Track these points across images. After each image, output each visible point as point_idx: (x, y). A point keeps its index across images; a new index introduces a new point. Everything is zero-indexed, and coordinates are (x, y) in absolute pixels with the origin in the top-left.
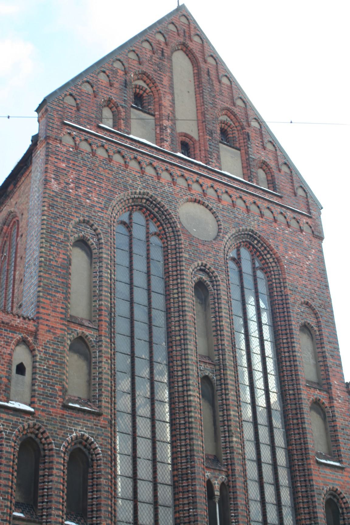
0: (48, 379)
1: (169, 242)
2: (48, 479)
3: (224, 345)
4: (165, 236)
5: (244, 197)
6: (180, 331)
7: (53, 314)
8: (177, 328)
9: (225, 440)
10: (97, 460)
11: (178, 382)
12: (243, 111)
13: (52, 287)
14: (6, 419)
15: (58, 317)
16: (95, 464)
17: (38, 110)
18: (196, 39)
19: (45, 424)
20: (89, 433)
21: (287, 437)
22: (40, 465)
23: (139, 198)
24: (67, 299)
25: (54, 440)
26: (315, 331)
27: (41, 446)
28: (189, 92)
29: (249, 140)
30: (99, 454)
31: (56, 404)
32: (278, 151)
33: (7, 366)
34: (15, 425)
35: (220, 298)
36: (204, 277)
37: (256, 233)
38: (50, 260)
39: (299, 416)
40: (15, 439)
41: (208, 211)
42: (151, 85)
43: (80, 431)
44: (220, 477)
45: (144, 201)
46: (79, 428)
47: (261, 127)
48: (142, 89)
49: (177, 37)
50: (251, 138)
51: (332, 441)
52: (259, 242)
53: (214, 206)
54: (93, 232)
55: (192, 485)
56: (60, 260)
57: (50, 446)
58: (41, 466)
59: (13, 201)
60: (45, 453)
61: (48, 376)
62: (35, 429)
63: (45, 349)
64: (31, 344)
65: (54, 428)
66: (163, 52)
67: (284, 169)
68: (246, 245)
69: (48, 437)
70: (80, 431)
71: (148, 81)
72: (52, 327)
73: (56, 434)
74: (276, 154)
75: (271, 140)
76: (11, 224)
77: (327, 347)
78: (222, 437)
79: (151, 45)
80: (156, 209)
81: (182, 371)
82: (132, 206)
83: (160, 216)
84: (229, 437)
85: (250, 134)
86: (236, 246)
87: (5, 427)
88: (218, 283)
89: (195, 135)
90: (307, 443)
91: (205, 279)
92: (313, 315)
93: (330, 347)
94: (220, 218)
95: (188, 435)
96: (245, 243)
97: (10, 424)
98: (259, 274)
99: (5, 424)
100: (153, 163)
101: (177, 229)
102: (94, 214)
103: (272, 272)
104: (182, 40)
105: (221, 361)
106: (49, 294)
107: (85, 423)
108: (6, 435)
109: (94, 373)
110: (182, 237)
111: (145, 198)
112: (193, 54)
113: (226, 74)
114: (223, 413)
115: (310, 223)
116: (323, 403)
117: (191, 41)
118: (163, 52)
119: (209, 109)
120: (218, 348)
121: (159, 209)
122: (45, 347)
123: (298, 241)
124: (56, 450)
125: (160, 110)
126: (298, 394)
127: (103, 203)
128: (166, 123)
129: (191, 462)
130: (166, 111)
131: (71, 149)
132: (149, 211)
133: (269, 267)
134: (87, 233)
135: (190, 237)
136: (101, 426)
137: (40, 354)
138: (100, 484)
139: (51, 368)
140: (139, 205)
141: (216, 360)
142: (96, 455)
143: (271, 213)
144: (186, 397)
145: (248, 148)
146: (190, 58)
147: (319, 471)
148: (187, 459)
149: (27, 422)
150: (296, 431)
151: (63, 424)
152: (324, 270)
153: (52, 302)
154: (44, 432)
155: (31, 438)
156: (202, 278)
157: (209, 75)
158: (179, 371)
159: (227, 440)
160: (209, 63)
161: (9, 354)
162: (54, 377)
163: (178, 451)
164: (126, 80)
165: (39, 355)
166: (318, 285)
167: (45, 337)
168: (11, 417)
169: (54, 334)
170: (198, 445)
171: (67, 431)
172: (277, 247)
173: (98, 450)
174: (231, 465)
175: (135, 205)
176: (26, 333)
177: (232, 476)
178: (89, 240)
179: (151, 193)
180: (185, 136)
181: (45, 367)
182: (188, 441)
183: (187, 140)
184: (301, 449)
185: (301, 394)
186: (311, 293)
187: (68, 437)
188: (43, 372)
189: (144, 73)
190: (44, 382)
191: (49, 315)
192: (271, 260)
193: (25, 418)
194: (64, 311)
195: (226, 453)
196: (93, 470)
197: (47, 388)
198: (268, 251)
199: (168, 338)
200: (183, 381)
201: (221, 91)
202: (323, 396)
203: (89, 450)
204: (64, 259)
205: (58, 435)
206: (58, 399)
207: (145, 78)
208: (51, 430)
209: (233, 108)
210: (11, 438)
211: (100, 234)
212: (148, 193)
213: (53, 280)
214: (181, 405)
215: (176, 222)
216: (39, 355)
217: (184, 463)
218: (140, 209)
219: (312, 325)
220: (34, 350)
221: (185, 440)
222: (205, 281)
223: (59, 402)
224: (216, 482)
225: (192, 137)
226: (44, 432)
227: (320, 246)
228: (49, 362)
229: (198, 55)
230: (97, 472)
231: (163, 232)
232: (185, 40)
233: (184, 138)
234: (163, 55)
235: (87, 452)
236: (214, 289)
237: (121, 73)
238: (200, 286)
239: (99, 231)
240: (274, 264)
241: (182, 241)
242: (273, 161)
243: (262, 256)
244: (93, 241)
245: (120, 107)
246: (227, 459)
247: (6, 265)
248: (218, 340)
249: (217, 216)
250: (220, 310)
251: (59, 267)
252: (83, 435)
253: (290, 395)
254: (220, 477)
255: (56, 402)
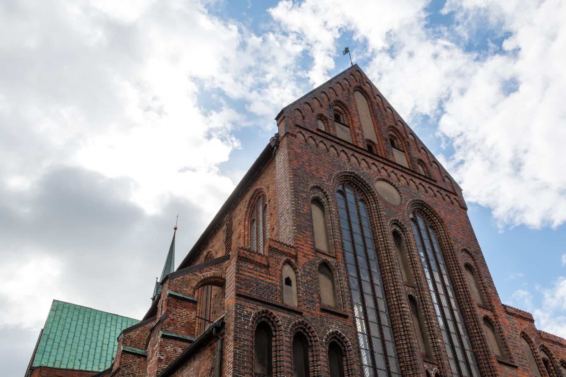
0: (308, 289)
1: (371, 205)
2: (317, 364)
3: (419, 273)
4: (367, 201)
5: (413, 180)
6: (388, 263)
7: (306, 245)
8: (386, 261)
9: (432, 341)
10: (349, 351)
11: (393, 298)
12: (402, 128)
13: (303, 227)
14: (283, 317)
15: (309, 247)
16: (348, 354)
17: (277, 119)
18: (367, 85)
19: (310, 322)
20: (341, 330)
21: (471, 342)
22: (309, 353)
23: (348, 175)
24: (313, 235)
25: (318, 334)
26: (475, 269)
27: (308, 339)
28: (367, 115)
29: (409, 146)
30: (349, 346)
31: (316, 308)
32: (428, 154)
33: (280, 278)
34: (290, 321)
35: (411, 243)
36: (397, 229)
37: (425, 202)
38: (299, 210)
39: (477, 327)
40: (290, 331)
41: (392, 187)
42: (345, 109)
43: (334, 328)
44: (434, 369)
45: (352, 178)
46: (334, 326)
47: (415, 139)
48: (339, 112)
49: (356, 83)
50: (410, 145)
51: (503, 347)
52: (427, 208)
53: (396, 184)
54: (323, 194)
55: (417, 374)
56: (306, 210)
57: (315, 338)
58: (310, 354)
59: (259, 182)
60: (312, 344)
61: (308, 288)
62: (303, 325)
63: (303, 269)
64: (294, 264)
65: (317, 325)
66: (349, 90)
67: (434, 165)
68: (419, 211)
69: (313, 332)
70: (334, 328)
71: (343, 107)
72: (307, 254)
73: (319, 329)
74: (427, 155)
75: (422, 146)
76: (257, 198)
77: (485, 280)
78: (430, 339)
79: (341, 85)
80: (360, 184)
81: (395, 290)
82: (344, 181)
83: (363, 188)
84: (435, 339)
85: (409, 142)
86: (413, 211)
87: (283, 322)
88: (407, 233)
89: (375, 141)
90: (488, 347)
91: (398, 230)
92: (471, 259)
93: (487, 280)
94: (401, 191)
95: (407, 336)
96: (418, 210)
97: (286, 320)
98: (430, 231)
99: (283, 320)
100: (355, 154)
101: (376, 196)
102: (322, 182)
103: (439, 229)
104: (358, 84)
105: (419, 284)
106: (301, 232)
107: (337, 323)
108: (284, 328)
109: (337, 288)
110: (380, 201)
111: (352, 176)
112: (366, 93)
113: (388, 106)
114: (427, 321)
115: (457, 199)
116: (491, 319)
117: (365, 86)
118: (349, 90)
119: (382, 125)
120: (415, 276)
121: (362, 183)
122: (304, 268)
123: (452, 209)
124: (320, 341)
125: (353, 124)
126: (474, 311)
127: (328, 176)
128: (357, 131)
129: (413, 356)
130: (356, 125)
131: (303, 142)
132: (355, 185)
133: (436, 226)
134: (319, 194)
135: (385, 202)
136: (348, 326)
137: (301, 271)
138: (354, 369)
139: (309, 282)
140: (348, 181)
141: (415, 284)
142: (348, 347)
143: (432, 191)
144: (401, 308)
145: (410, 150)
146: (364, 96)
147: (500, 368)
148: (410, 354)
149: (297, 319)
150: (478, 338)
151: (322, 322)
152: (472, 229)
153: (304, 237)
154: (310, 328)
155: (300, 332)
156: (396, 229)
157: (378, 106)
158: (393, 290)
159: (434, 341)
160: (377, 99)
161: (280, 270)
162: (312, 289)
163: (401, 348)
164: (330, 104)
165: (300, 272)
166: (470, 239)
167: (302, 260)
168: (286, 315)
169: (308, 258)
170: (415, 343)
171: (326, 328)
172: (440, 212)
173: (349, 343)
174: (440, 359)
175: (346, 181)
176: (289, 256)
177: (443, 368)
178: (321, 199)
179: (356, 173)
180: (369, 142)
181: (305, 281)
182: (408, 340)
183: (371, 144)
184: (484, 351)
185: (476, 311)
186: (467, 243)
187: (327, 332)
188: (304, 284)
189: (339, 101)
190: (306, 292)
191: (303, 245)
192: (437, 221)
193: (296, 316)
194: (312, 243)
195: (435, 351)
196: (346, 358)
197: (308, 295)
198: (434, 215)
199: (380, 268)
200: (396, 297)
201: (387, 116)
202: (489, 314)
203: (308, 333)
204: (308, 210)
205: (320, 330)
206: (316, 304)
207: (340, 105)
208: (315, 326)
209: (396, 126)
210: (288, 331)
211: (328, 195)
212: (354, 173)
213: (303, 222)
214: (398, 314)
215: (374, 192)
216: (300, 272)
217: (407, 356)
218: (349, 184)
219: (472, 265)
220: (296, 268)
221: (406, 339)
222: (399, 232)
223: (318, 306)
224: (432, 372)
225: (374, 142)
226: (310, 328)
227: (466, 214)
228: (307, 277)
229: (370, 94)
230: (350, 360)
231: (366, 199)
232: (361, 84)
233: (368, 142)
234: (349, 92)
235: (340, 345)
236: (405, 237)
237: (326, 99)
238: (396, 234)
239: (328, 193)
240: (439, 224)
241: (381, 204)
242: (426, 160)
243: (431, 218)
244: (324, 200)
245: (329, 120)
246: (436, 356)
247: (255, 224)
248: (414, 270)
249: (399, 190)
250: (412, 250)
251: (305, 214)
252: (337, 332)
253: (467, 312)
254: (434, 369)
255: (316, 306)
